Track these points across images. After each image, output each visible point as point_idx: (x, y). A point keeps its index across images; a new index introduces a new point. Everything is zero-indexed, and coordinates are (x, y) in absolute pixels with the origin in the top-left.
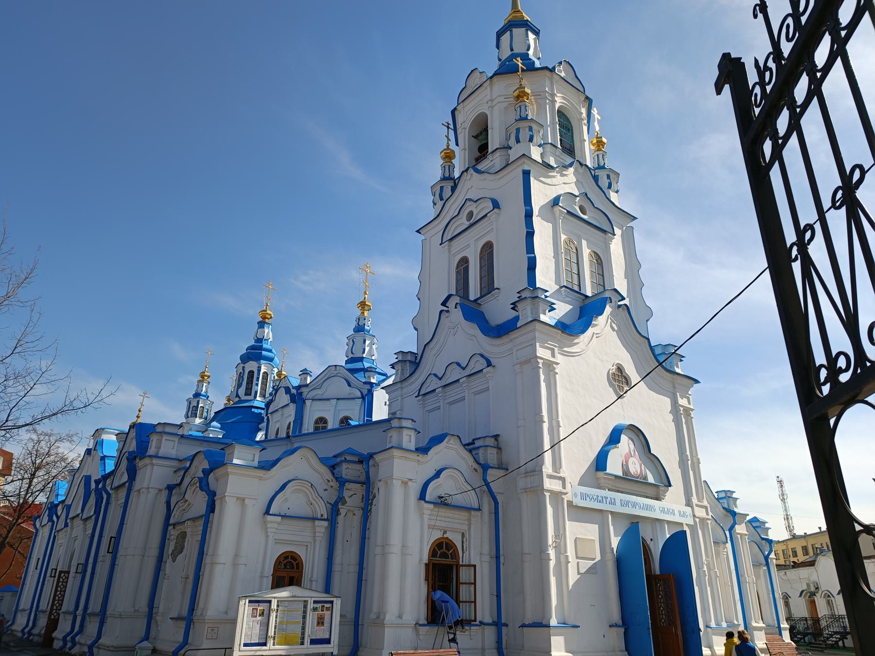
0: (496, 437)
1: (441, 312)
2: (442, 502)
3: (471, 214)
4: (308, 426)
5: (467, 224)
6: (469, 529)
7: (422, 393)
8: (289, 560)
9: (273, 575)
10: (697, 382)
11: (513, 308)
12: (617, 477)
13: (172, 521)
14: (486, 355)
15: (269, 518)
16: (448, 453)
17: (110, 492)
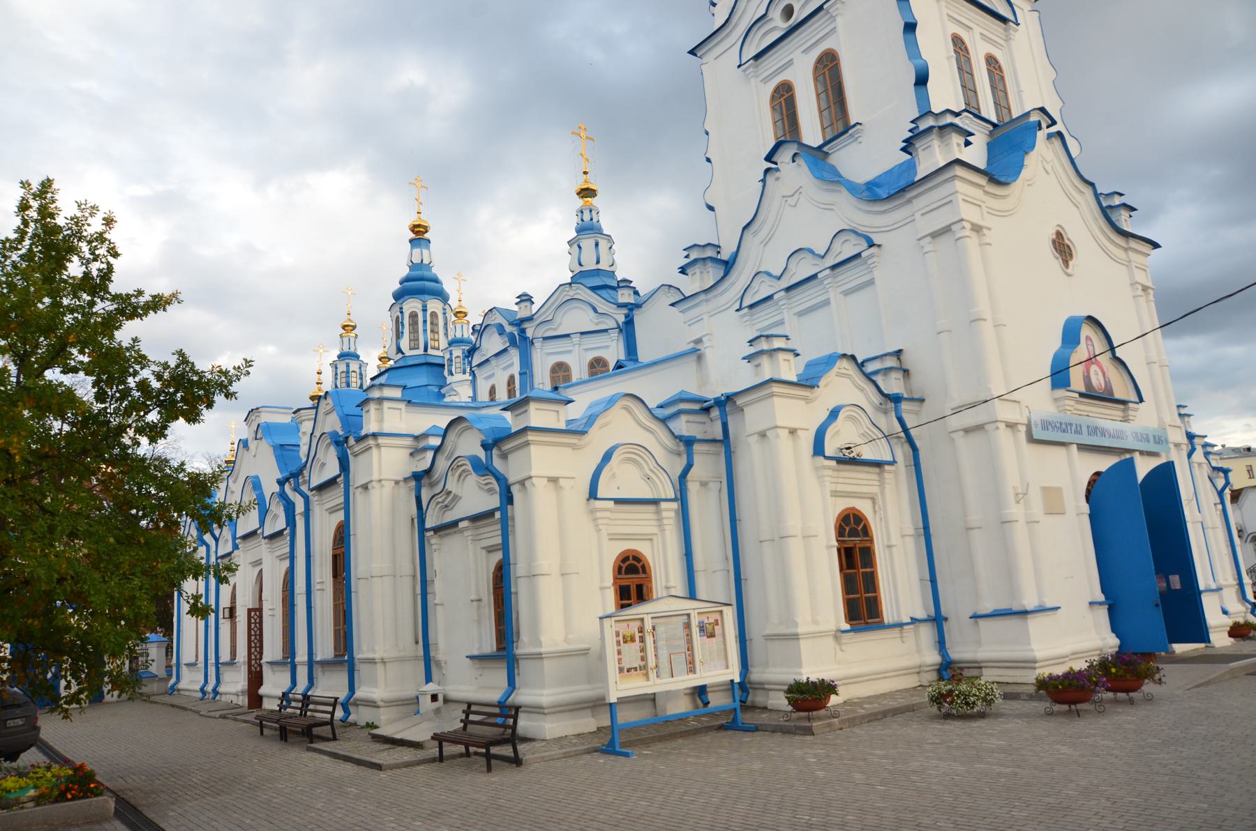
0: (898, 354)
1: (767, 171)
2: (848, 460)
3: (788, 12)
4: (542, 380)
5: (784, 26)
6: (883, 492)
7: (745, 304)
8: (631, 561)
9: (614, 583)
10: (1156, 245)
11: (903, 149)
12: (1081, 395)
13: (428, 525)
14: (861, 229)
15: (598, 504)
16: (842, 388)
17: (309, 493)
